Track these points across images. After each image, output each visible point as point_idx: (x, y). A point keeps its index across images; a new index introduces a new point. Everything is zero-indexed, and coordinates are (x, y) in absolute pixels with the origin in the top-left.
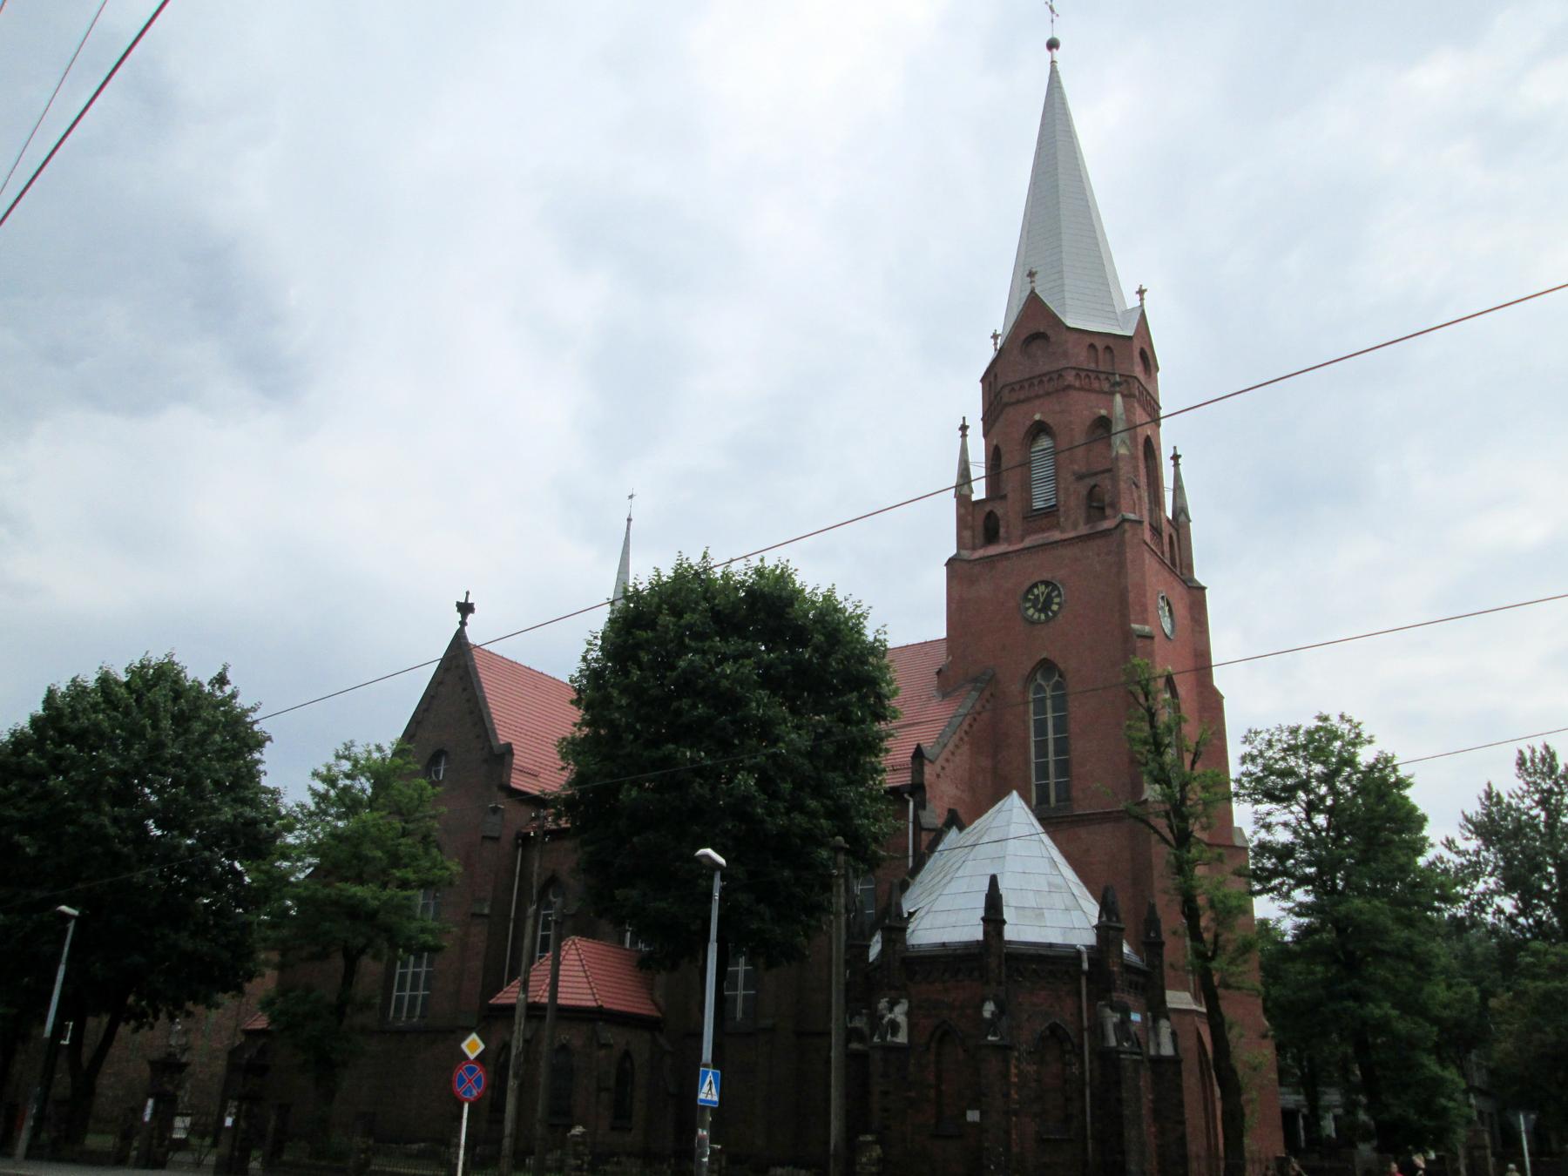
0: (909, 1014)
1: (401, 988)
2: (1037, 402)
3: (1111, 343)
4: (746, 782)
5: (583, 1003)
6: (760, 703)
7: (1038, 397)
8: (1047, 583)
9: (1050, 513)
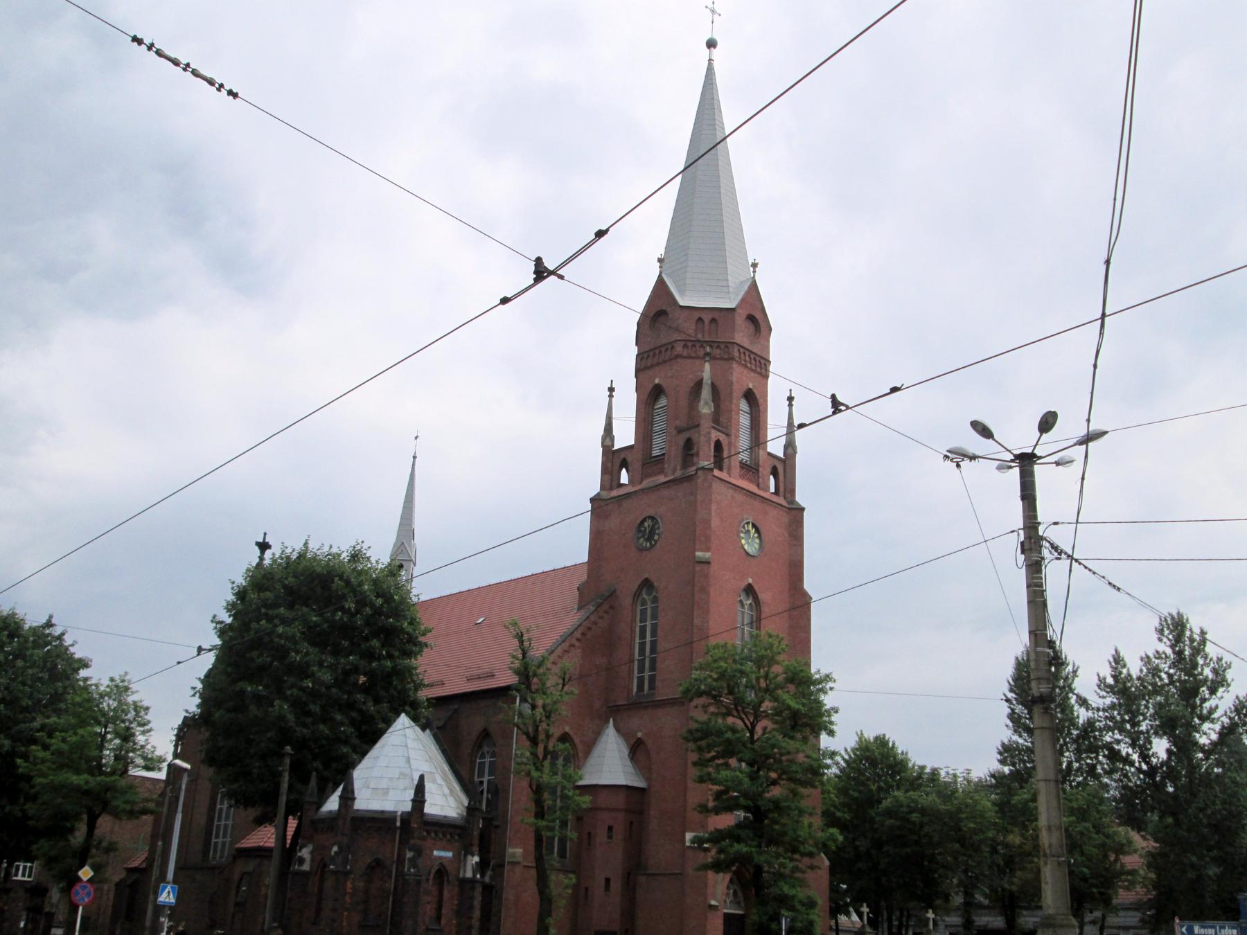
0: (312, 853)
1: (217, 837)
2: (657, 368)
3: (716, 315)
4: (281, 707)
6: (303, 653)
7: (658, 364)
8: (652, 518)
9: (660, 459)
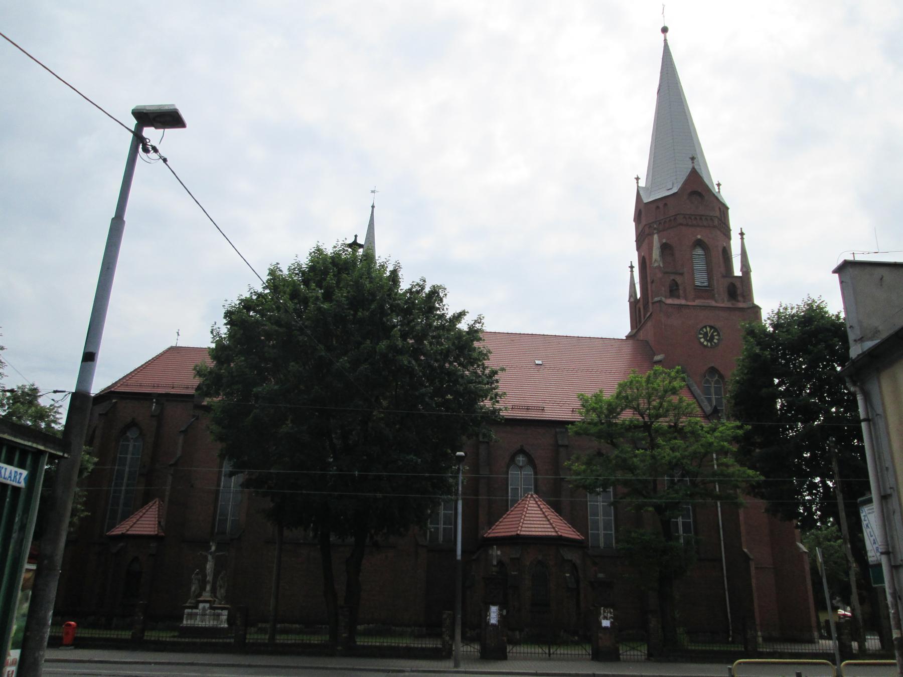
5: (550, 534)
